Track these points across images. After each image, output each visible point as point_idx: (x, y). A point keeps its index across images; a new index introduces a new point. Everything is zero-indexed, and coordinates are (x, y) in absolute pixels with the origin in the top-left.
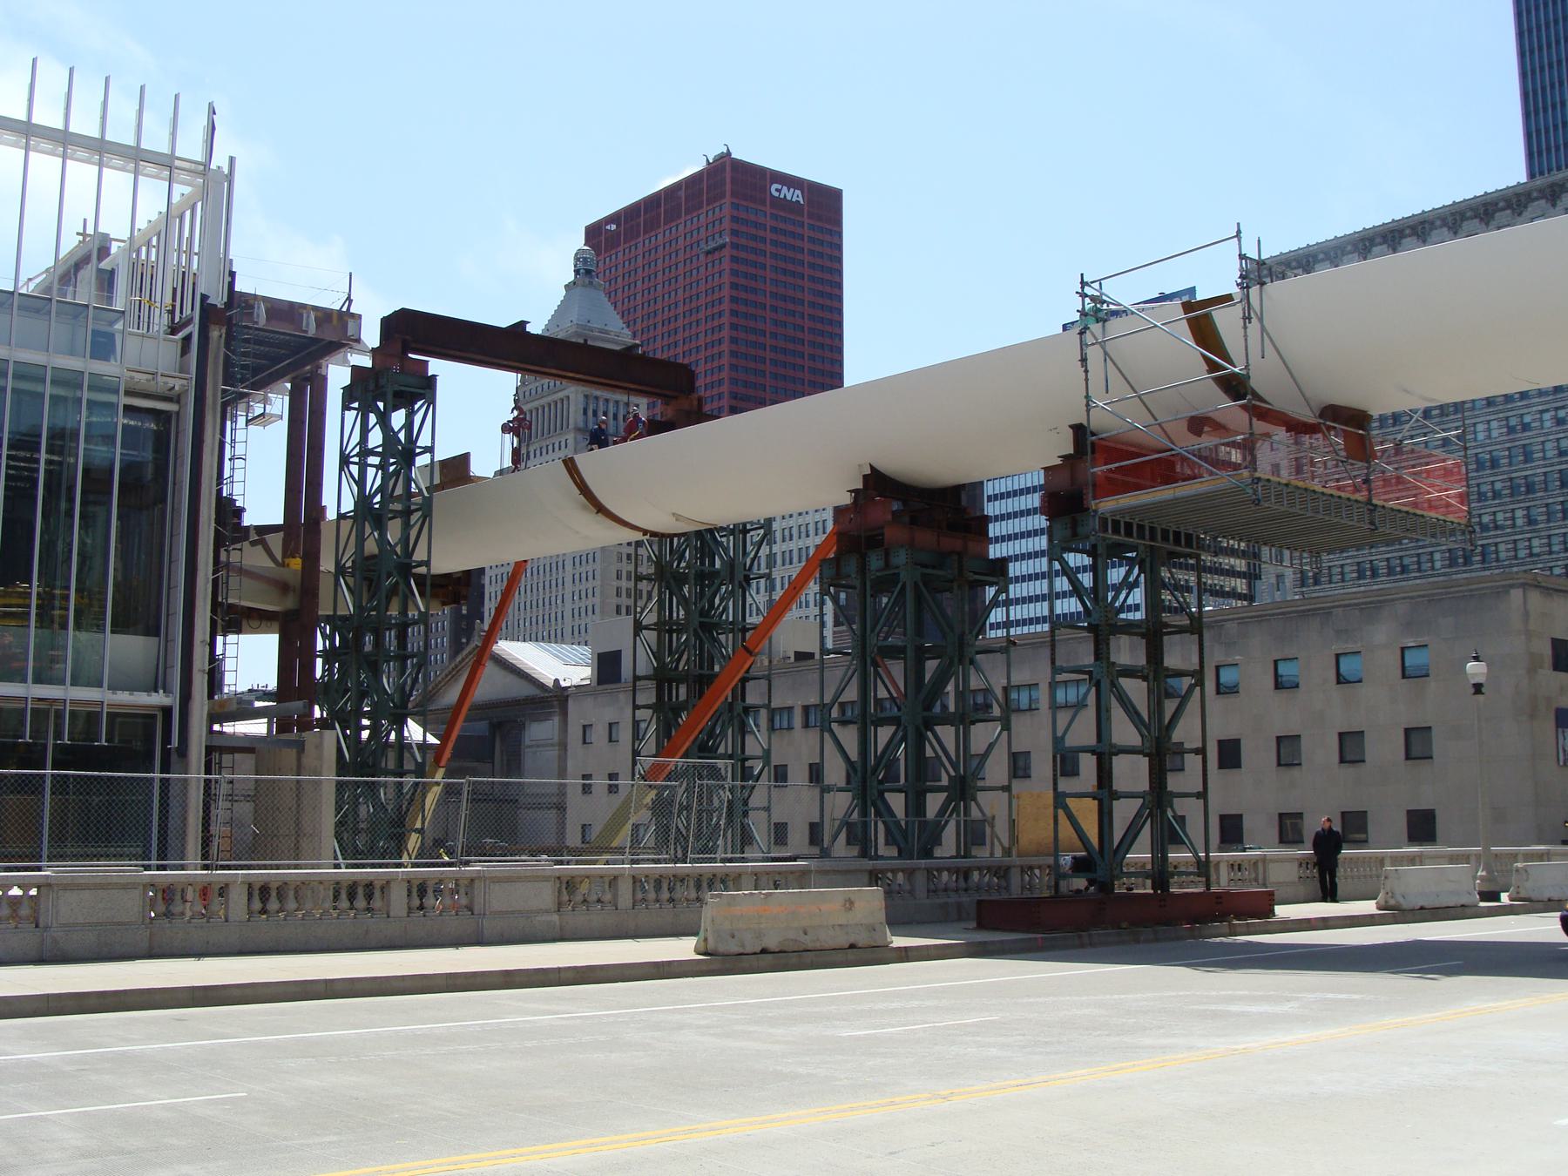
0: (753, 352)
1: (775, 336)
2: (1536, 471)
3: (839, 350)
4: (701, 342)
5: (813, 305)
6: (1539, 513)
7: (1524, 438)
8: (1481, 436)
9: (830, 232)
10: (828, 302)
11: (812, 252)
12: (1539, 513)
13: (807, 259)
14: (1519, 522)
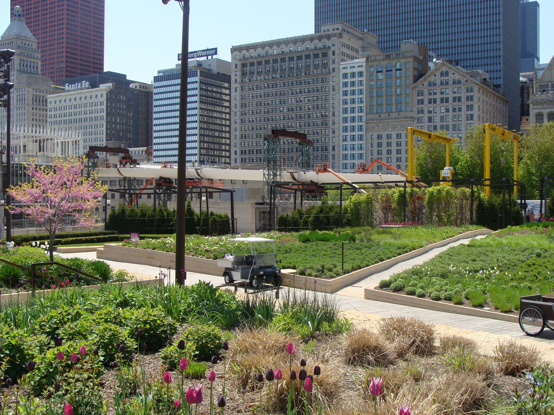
0: (74, 42)
1: (81, 37)
2: (302, 113)
3: (102, 42)
4: (56, 37)
5: (94, 27)
6: (302, 124)
7: (300, 104)
8: (290, 102)
9: (100, 24)
10: (99, 26)
11: (94, 8)
12: (302, 124)
13: (93, 10)
14: (298, 126)
